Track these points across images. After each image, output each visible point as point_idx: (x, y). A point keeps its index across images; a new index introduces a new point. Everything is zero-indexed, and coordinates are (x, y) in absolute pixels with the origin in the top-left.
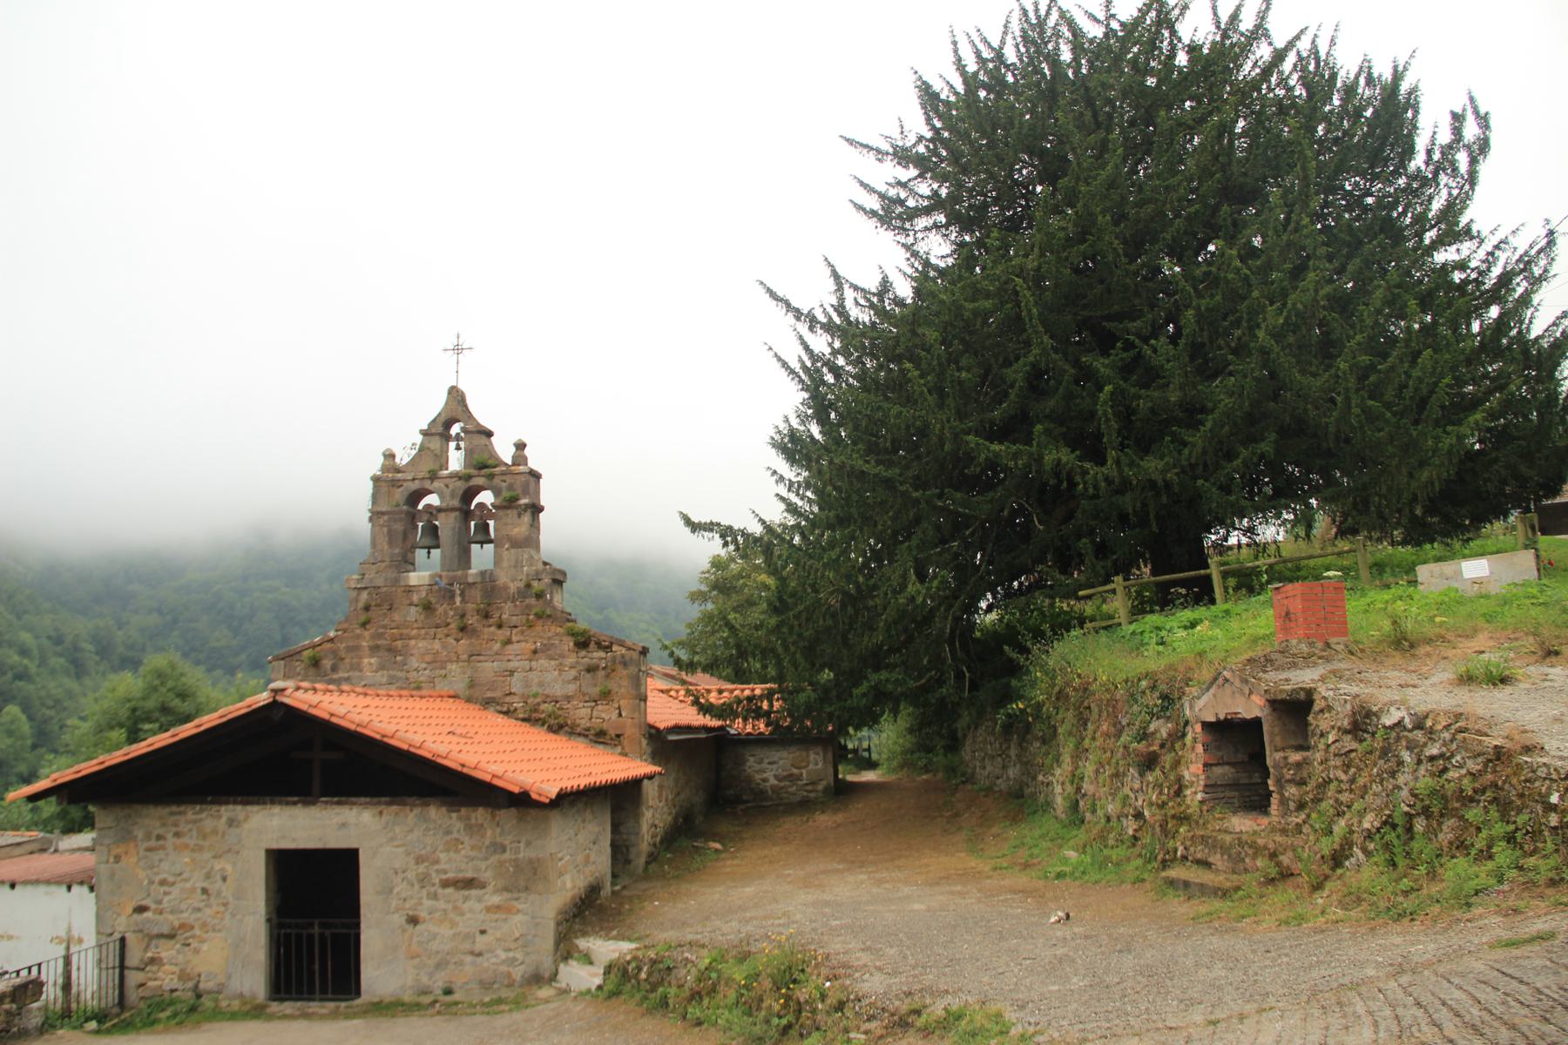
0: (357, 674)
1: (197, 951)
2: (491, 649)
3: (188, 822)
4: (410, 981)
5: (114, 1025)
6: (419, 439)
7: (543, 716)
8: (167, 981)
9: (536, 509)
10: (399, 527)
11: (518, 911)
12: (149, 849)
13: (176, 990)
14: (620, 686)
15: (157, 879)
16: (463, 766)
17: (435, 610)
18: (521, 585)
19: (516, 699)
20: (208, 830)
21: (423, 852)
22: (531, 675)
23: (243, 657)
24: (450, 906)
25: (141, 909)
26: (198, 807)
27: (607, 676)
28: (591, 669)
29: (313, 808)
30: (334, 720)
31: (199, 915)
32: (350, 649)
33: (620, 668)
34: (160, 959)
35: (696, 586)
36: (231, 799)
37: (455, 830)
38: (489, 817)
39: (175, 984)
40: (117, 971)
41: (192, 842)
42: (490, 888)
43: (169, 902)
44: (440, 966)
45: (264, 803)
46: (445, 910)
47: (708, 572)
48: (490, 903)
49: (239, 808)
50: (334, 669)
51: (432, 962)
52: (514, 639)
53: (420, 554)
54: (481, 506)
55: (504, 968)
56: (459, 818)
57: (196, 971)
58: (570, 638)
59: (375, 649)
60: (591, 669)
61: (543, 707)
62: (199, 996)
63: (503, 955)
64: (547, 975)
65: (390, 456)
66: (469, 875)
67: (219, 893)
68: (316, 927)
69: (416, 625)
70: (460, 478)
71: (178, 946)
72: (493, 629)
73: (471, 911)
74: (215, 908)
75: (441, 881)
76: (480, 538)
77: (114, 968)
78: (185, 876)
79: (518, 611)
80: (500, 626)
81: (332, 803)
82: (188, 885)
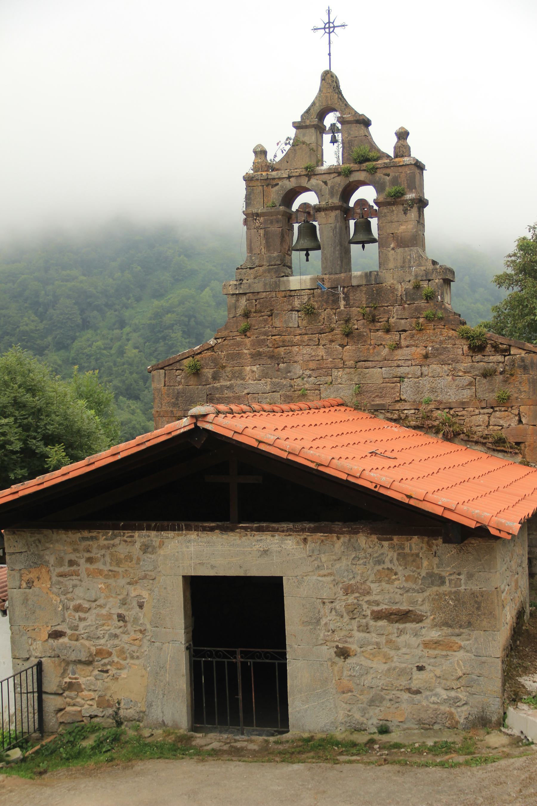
0: (240, 382)
1: (115, 678)
2: (379, 354)
3: (100, 548)
4: (341, 716)
5: (37, 753)
6: (292, 132)
7: (436, 423)
8: (86, 706)
9: (422, 203)
10: (275, 229)
11: (460, 647)
12: (61, 575)
13: (96, 716)
14: (520, 392)
15: (72, 605)
16: (410, 497)
17: (319, 314)
18: (410, 286)
19: (407, 406)
20: (122, 556)
21: (352, 582)
22: (423, 381)
23: (50, 339)
24: (383, 640)
25: (56, 635)
26: (111, 532)
27: (506, 381)
28: (487, 374)
29: (231, 534)
30: (262, 447)
31: (116, 642)
32: (231, 357)
33: (519, 371)
34: (79, 685)
35: (502, 269)
36: (183, 524)
37: (387, 560)
38: (425, 546)
39: (95, 710)
40: (36, 695)
41: (106, 568)
42: (427, 622)
43: (85, 628)
44: (372, 702)
45: (180, 529)
46: (377, 644)
47: (515, 255)
48: (427, 638)
49: (153, 533)
50: (216, 377)
51: (365, 698)
52: (403, 343)
53: (297, 257)
54: (362, 203)
55: (445, 708)
56: (392, 547)
57: (115, 698)
58: (464, 341)
59: (256, 356)
60: (487, 374)
61: (438, 413)
62: (119, 724)
63: (444, 695)
64: (494, 718)
65: (261, 153)
66: (404, 607)
67: (136, 620)
68: (239, 656)
69: (298, 331)
70: (339, 174)
71: (96, 672)
72: (380, 333)
73: (407, 645)
74: (133, 635)
75: (373, 612)
76: (361, 237)
77: (33, 692)
78: (101, 602)
79: (406, 314)
80: (388, 331)
81: (252, 530)
82: (104, 611)
